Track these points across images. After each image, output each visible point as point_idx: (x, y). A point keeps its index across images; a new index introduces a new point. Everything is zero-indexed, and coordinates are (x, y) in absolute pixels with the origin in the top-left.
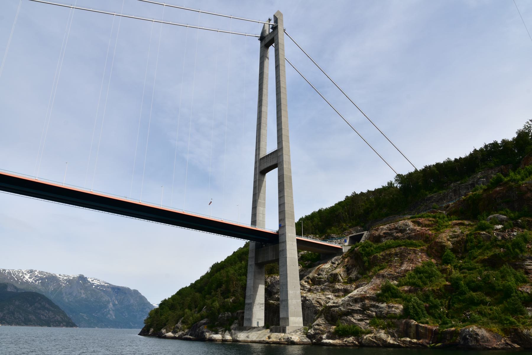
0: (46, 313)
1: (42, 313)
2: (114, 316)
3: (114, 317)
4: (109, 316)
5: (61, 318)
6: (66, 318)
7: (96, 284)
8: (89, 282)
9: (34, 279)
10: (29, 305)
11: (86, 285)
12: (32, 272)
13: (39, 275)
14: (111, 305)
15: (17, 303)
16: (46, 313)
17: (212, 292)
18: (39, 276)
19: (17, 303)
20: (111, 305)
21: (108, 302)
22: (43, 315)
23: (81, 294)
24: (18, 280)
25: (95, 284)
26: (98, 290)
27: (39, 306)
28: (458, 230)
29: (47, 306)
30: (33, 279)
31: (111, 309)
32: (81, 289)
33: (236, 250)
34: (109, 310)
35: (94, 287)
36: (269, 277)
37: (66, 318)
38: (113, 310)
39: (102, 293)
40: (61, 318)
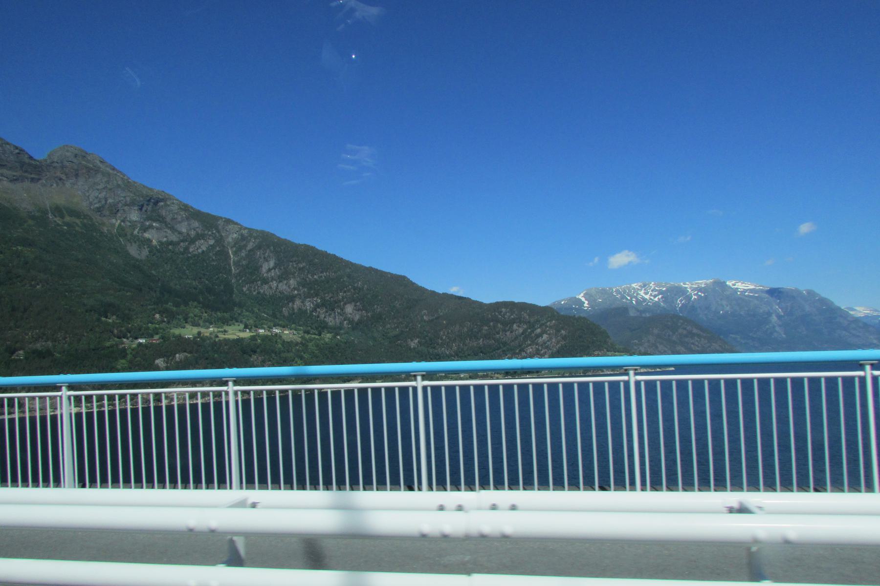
0: (697, 341)
1: (691, 342)
2: (784, 334)
3: (784, 336)
4: (775, 335)
5: (720, 346)
6: (726, 346)
7: (740, 289)
8: (730, 287)
9: (651, 294)
10: (671, 333)
11: (728, 293)
12: (646, 285)
13: (656, 288)
14: (774, 318)
15: (656, 331)
16: (697, 341)
17: (245, 287)
18: (657, 290)
19: (656, 331)
20: (774, 318)
21: (769, 314)
22: (693, 344)
23: (723, 306)
24: (631, 298)
25: (739, 290)
26: (747, 298)
27: (685, 332)
28: (50, 215)
29: (695, 331)
30: (649, 294)
31: (776, 325)
32: (721, 299)
33: (288, 239)
34: (774, 327)
35: (740, 294)
36: (294, 263)
37: (726, 346)
38: (780, 326)
39: (756, 302)
40: (720, 346)
